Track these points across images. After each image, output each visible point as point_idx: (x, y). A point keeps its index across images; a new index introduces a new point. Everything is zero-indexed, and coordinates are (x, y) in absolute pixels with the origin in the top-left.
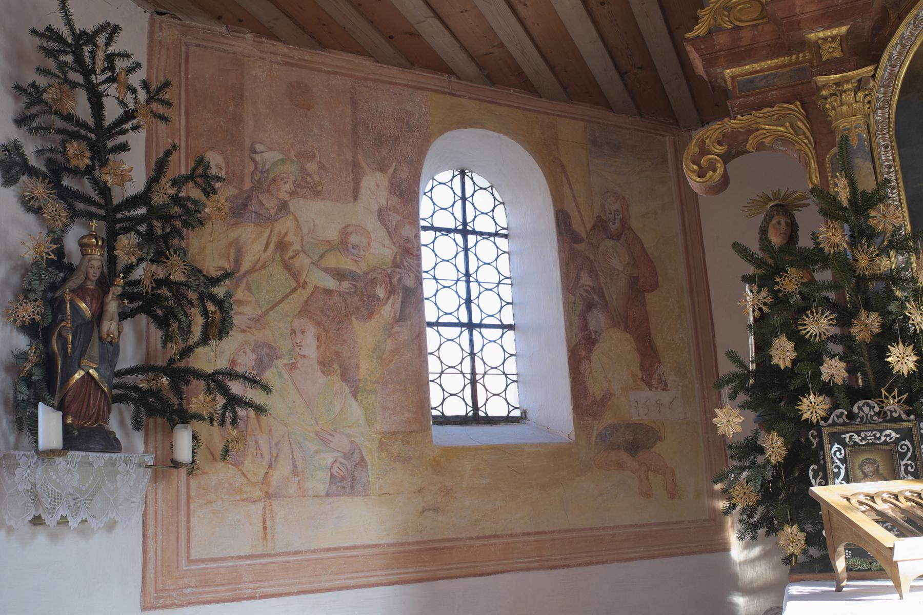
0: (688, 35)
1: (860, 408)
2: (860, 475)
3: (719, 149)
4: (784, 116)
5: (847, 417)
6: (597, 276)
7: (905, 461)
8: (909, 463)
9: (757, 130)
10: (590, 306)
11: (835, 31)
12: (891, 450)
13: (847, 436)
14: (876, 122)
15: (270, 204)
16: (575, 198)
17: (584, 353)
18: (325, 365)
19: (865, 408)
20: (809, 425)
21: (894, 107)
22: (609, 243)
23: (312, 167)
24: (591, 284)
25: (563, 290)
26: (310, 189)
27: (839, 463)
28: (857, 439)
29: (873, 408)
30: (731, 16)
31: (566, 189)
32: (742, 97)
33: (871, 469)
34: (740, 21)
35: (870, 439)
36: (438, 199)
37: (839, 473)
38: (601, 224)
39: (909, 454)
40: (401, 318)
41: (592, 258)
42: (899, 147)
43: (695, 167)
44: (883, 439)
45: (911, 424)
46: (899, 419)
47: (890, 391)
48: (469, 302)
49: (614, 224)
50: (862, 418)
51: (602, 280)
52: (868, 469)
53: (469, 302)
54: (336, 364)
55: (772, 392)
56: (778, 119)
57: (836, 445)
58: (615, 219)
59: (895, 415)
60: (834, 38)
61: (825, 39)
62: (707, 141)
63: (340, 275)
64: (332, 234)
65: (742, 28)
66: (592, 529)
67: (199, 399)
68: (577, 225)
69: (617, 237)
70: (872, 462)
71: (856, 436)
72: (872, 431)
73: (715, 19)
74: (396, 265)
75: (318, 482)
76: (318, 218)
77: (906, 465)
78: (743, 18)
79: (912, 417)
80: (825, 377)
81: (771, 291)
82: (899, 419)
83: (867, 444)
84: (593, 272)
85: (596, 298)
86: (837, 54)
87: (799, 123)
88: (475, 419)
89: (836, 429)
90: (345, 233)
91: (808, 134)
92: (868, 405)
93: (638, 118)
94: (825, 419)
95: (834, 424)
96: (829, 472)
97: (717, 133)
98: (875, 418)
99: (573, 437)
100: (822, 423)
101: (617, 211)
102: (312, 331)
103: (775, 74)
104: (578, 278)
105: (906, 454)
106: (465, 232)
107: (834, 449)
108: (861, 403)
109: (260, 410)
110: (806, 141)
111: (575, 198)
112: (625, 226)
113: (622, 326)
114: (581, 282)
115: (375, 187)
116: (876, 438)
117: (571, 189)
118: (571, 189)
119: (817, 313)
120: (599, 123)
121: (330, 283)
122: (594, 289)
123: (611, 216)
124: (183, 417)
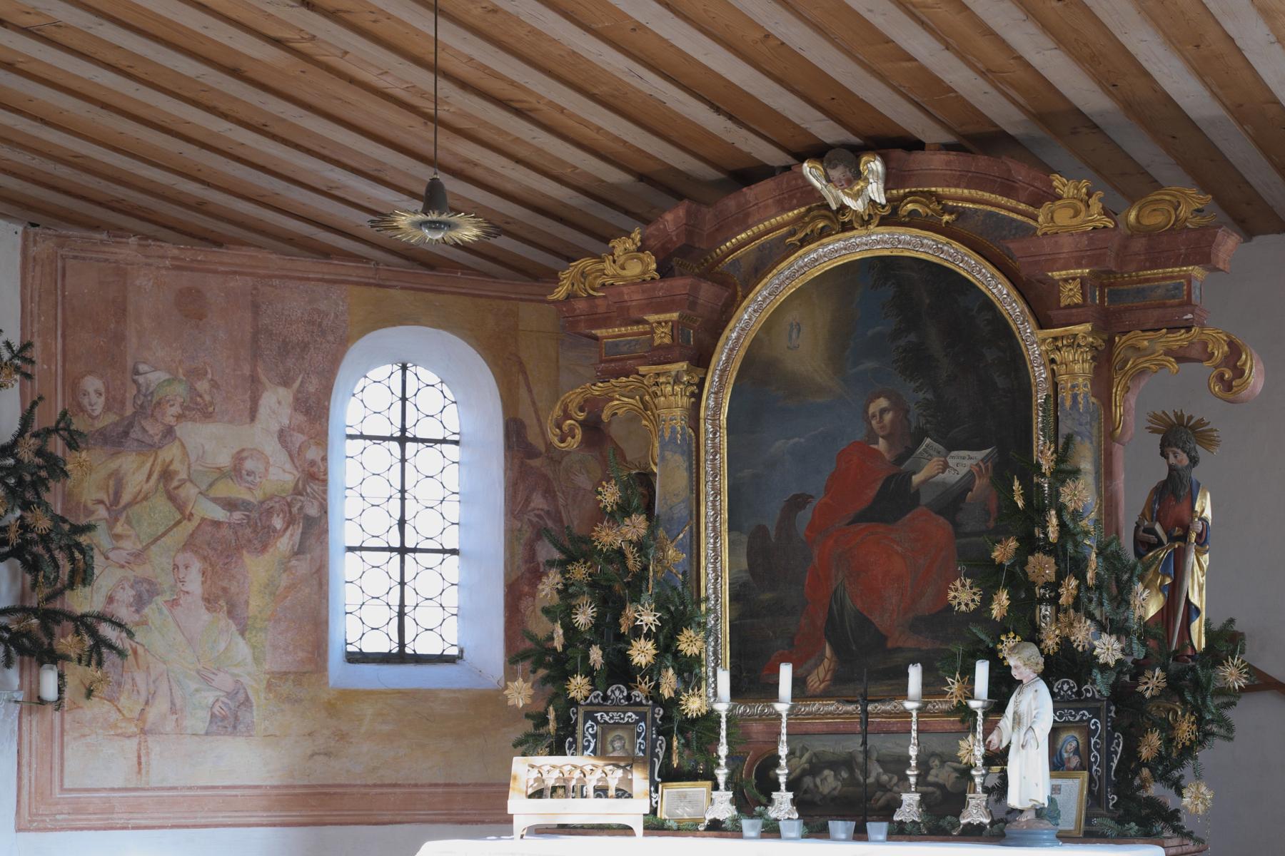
1: (613, 692)
3: (581, 416)
6: (554, 497)
9: (612, 399)
15: (154, 429)
16: (534, 403)
17: (526, 589)
18: (210, 601)
19: (617, 692)
20: (574, 702)
23: (203, 386)
24: (546, 508)
25: (506, 515)
26: (199, 410)
28: (607, 718)
31: (523, 392)
36: (368, 395)
37: (588, 747)
40: (300, 551)
41: (551, 475)
47: (643, 677)
48: (402, 523)
51: (561, 501)
53: (402, 523)
54: (222, 600)
61: (659, 323)
63: (230, 505)
64: (224, 460)
67: (67, 642)
70: (621, 738)
74: (298, 492)
75: (198, 721)
76: (209, 443)
82: (640, 704)
84: (549, 493)
86: (667, 340)
88: (400, 657)
89: (590, 708)
90: (239, 458)
94: (586, 698)
102: (196, 566)
103: (637, 341)
104: (528, 501)
106: (403, 440)
108: (614, 687)
109: (121, 653)
111: (534, 403)
114: (532, 505)
115: (276, 405)
117: (530, 391)
118: (530, 391)
121: (220, 514)
122: (548, 513)
124: (51, 656)
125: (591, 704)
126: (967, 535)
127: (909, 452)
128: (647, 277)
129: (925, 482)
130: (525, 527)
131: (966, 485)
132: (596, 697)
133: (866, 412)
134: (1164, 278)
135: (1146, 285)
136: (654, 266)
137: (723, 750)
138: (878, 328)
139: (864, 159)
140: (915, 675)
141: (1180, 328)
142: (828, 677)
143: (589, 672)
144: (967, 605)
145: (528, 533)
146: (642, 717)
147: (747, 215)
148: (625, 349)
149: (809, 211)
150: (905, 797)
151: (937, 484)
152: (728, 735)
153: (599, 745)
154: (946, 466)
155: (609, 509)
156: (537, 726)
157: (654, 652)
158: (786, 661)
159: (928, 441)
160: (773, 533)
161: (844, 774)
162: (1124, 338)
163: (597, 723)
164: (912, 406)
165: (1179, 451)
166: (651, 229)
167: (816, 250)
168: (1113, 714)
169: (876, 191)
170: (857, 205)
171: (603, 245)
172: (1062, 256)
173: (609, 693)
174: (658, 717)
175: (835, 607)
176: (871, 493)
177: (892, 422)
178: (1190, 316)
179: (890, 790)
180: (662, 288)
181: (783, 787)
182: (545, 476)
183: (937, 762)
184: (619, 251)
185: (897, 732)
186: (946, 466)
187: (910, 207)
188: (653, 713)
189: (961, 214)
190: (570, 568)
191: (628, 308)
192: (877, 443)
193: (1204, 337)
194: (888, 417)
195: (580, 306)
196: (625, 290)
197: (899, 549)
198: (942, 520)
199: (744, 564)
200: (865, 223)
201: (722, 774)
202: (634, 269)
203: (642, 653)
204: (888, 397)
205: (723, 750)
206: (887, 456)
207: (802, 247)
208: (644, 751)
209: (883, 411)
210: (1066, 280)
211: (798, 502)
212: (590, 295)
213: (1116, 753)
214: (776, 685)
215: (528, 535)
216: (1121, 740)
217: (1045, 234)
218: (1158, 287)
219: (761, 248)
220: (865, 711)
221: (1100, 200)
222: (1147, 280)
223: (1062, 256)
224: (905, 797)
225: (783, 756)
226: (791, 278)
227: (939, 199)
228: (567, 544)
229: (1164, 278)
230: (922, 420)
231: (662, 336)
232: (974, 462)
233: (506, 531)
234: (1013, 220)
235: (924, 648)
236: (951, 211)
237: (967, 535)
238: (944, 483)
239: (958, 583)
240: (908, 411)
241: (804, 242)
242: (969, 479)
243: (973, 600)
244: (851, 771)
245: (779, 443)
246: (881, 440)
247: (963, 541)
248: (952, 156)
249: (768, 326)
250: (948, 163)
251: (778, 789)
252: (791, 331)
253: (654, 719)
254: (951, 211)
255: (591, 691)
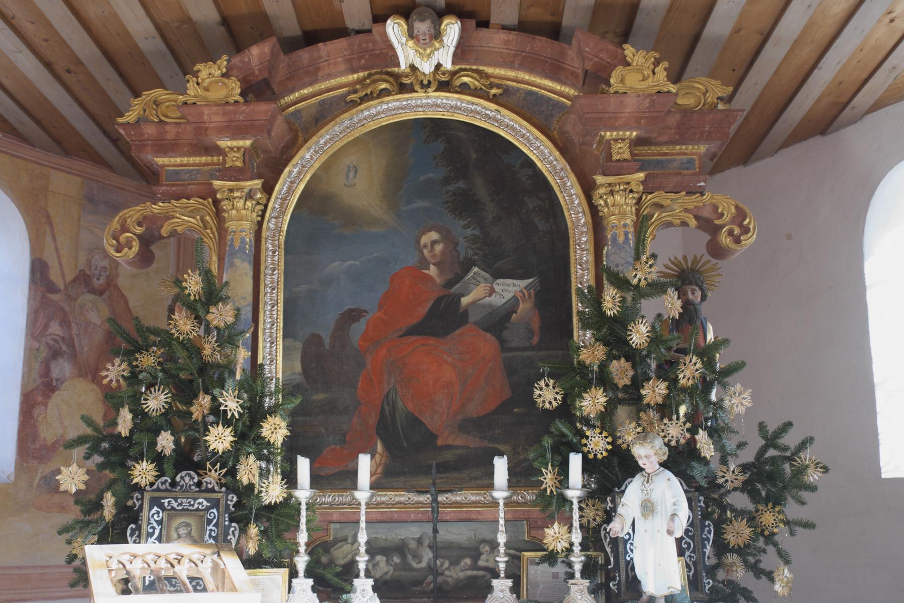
0: (120, 120)
1: (182, 478)
2: (175, 536)
3: (139, 230)
4: (198, 210)
5: (170, 484)
6: (69, 327)
7: (211, 527)
8: (213, 528)
9: (173, 217)
10: (55, 354)
11: (241, 143)
12: (202, 516)
13: (166, 501)
14: (268, 229)
16: (57, 250)
17: (40, 399)
19: (187, 478)
20: (137, 488)
21: (288, 218)
22: (90, 297)
24: (61, 334)
25: (27, 336)
27: (155, 524)
28: (175, 505)
29: (193, 478)
30: (159, 110)
31: (49, 240)
32: (167, 185)
33: (185, 531)
34: (166, 116)
35: (186, 505)
37: (153, 533)
38: (83, 279)
39: (215, 521)
41: (67, 309)
42: (286, 254)
43: (114, 242)
44: (196, 506)
45: (219, 496)
46: (212, 490)
47: (213, 465)
49: (98, 279)
50: (182, 487)
51: (75, 331)
52: (183, 531)
55: (116, 453)
56: (191, 211)
57: (156, 508)
58: (100, 275)
59: (210, 486)
60: (239, 148)
61: (231, 148)
62: (129, 220)
65: (167, 123)
66: (19, 568)
68: (55, 275)
69: (100, 293)
70: (187, 525)
71: (173, 502)
72: (187, 498)
73: (145, 110)
77: (211, 530)
78: (169, 114)
79: (224, 489)
80: (159, 448)
81: (130, 365)
82: (212, 490)
83: (183, 510)
84: (65, 322)
85: (64, 348)
86: (239, 164)
87: (208, 218)
89: (157, 494)
91: (214, 229)
92: (190, 475)
93: (144, 183)
94: (152, 484)
95: (158, 490)
96: (144, 532)
97: (139, 214)
98: (193, 487)
99: (12, 478)
100: (148, 488)
101: (105, 268)
103: (199, 170)
104: (46, 327)
105: (212, 520)
107: (153, 511)
108: (184, 473)
110: (211, 235)
111: (57, 250)
112: (111, 283)
113: (90, 377)
114: (50, 331)
116: (190, 505)
117: (54, 239)
118: (54, 239)
119: (159, 390)
120: (99, 182)
122: (63, 339)
123: (97, 272)
125: (158, 490)
126: (512, 349)
127: (458, 278)
128: (231, 100)
129: (473, 303)
130: (43, 347)
131: (511, 307)
132: (163, 483)
133: (418, 242)
134: (679, 154)
135: (664, 158)
136: (239, 91)
137: (303, 537)
138: (430, 175)
139: (445, 22)
140: (501, 466)
141: (694, 193)
142: (379, 470)
143: (158, 459)
144: (550, 403)
145: (44, 353)
146: (215, 504)
147: (318, 69)
148: (186, 176)
149: (370, 75)
150: (495, 582)
151: (484, 306)
152: (308, 522)
153: (164, 532)
154: (492, 291)
155: (192, 298)
156: (86, 512)
157: (233, 439)
158: (364, 451)
159: (476, 269)
160: (327, 342)
161: (396, 560)
162: (650, 197)
163: (163, 508)
164: (461, 240)
165: (697, 289)
166: (236, 60)
167: (375, 107)
168: (702, 504)
169: (445, 56)
170: (426, 68)
171: (181, 74)
172: (623, 115)
173: (178, 478)
174: (231, 504)
175: (387, 408)
176: (423, 311)
177: (443, 252)
178: (702, 184)
179: (442, 574)
180: (243, 112)
181: (362, 574)
182: (62, 309)
183: (487, 548)
184: (203, 74)
185: (447, 521)
186: (492, 291)
187: (466, 79)
188: (227, 500)
189: (507, 91)
190: (138, 356)
191: (206, 129)
192: (428, 269)
193: (714, 201)
194: (439, 248)
195: (150, 131)
196: (206, 111)
197: (449, 360)
198: (489, 335)
199: (298, 367)
200: (425, 87)
201: (302, 561)
202: (217, 94)
203: (220, 439)
204: (439, 231)
205: (303, 537)
206: (438, 280)
207: (360, 104)
208: (215, 539)
209: (434, 243)
210: (616, 140)
211: (352, 316)
212: (161, 121)
213: (708, 539)
214: (355, 473)
215: (44, 355)
216: (712, 528)
217: (616, 92)
218: (674, 160)
219: (322, 103)
220: (435, 500)
221: (665, 69)
222: (665, 154)
223: (623, 115)
224: (495, 582)
225: (502, 544)
226: (352, 127)
227: (488, 76)
228: (135, 335)
229: (679, 154)
230: (470, 252)
231: (235, 160)
232: (518, 289)
233: (25, 349)
234: (550, 99)
235: (472, 446)
236: (498, 86)
237: (512, 349)
238: (490, 305)
239: (542, 383)
240: (457, 244)
241: (363, 100)
242: (514, 303)
243: (555, 399)
244: (403, 556)
245: (335, 264)
246: (432, 266)
247: (510, 354)
248: (512, 36)
249: (326, 167)
250: (507, 42)
251: (357, 576)
252: (349, 171)
253: (227, 506)
254: (498, 86)
255: (158, 477)
